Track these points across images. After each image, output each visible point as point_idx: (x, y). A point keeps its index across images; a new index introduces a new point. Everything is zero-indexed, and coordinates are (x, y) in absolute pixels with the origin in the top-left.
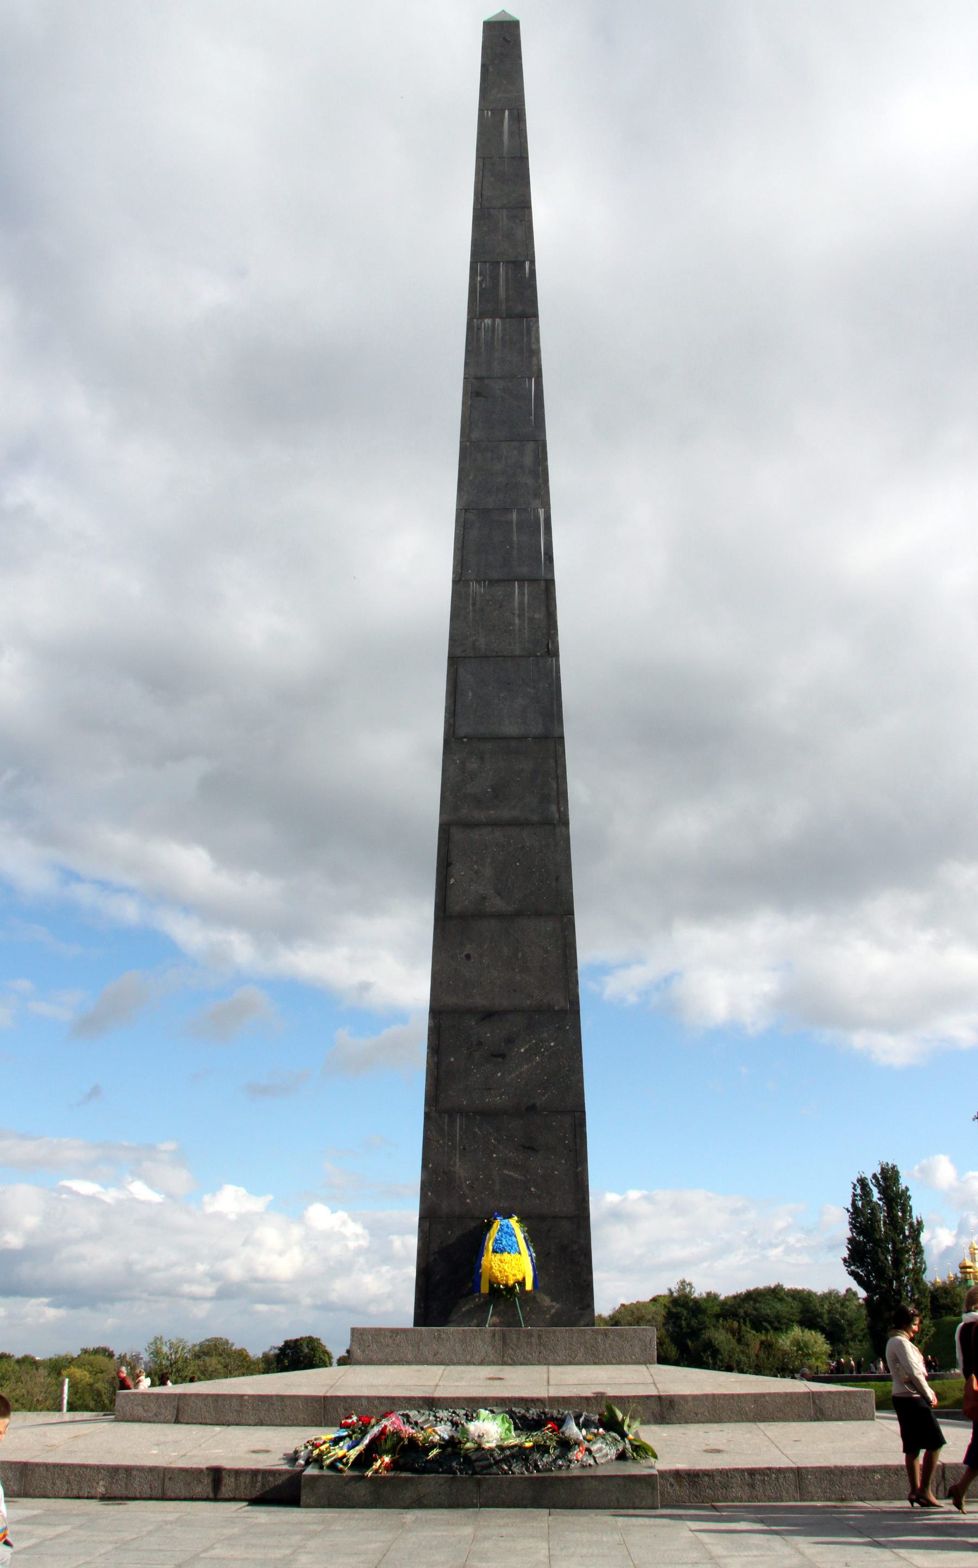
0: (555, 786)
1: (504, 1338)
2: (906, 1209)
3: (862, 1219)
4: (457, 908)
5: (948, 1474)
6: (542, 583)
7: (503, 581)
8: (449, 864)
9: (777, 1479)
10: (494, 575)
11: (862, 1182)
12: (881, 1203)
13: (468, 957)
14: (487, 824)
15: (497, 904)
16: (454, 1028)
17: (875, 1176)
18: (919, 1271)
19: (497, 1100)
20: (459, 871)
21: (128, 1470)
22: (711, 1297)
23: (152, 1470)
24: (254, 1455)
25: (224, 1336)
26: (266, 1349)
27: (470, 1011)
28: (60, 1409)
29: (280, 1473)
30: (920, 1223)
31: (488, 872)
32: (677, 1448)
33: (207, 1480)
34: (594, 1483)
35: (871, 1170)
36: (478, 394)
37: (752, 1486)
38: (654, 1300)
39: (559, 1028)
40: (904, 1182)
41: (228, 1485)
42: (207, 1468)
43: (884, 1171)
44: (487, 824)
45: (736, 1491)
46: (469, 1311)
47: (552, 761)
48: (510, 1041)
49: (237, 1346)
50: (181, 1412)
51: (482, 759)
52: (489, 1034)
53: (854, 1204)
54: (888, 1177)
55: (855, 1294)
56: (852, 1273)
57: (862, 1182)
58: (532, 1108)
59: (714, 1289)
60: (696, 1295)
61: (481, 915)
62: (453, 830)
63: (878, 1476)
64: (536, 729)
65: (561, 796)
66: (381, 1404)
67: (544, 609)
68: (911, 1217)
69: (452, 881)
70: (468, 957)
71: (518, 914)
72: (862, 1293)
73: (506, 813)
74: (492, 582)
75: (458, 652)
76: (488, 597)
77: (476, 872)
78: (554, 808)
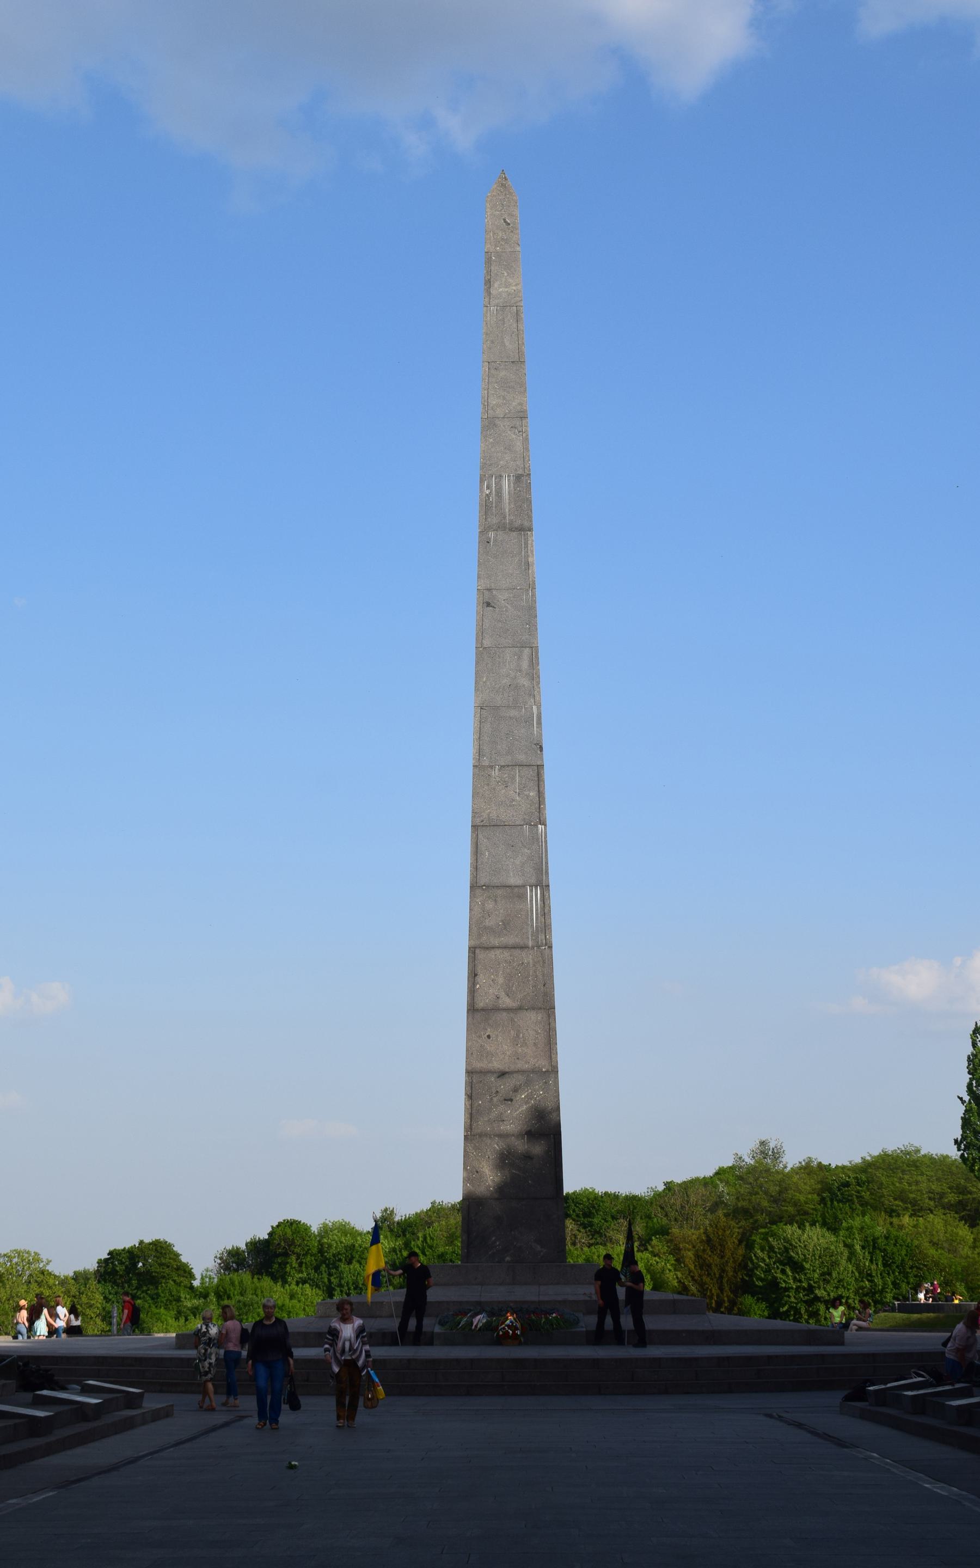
13: (489, 1037)
15: (506, 1002)
31: (501, 980)
36: (488, 605)
48: (516, 1090)
51: (496, 901)
52: (504, 1086)
61: (496, 1009)
62: (477, 951)
70: (489, 1037)
71: (520, 1008)
73: (511, 940)
75: (478, 821)
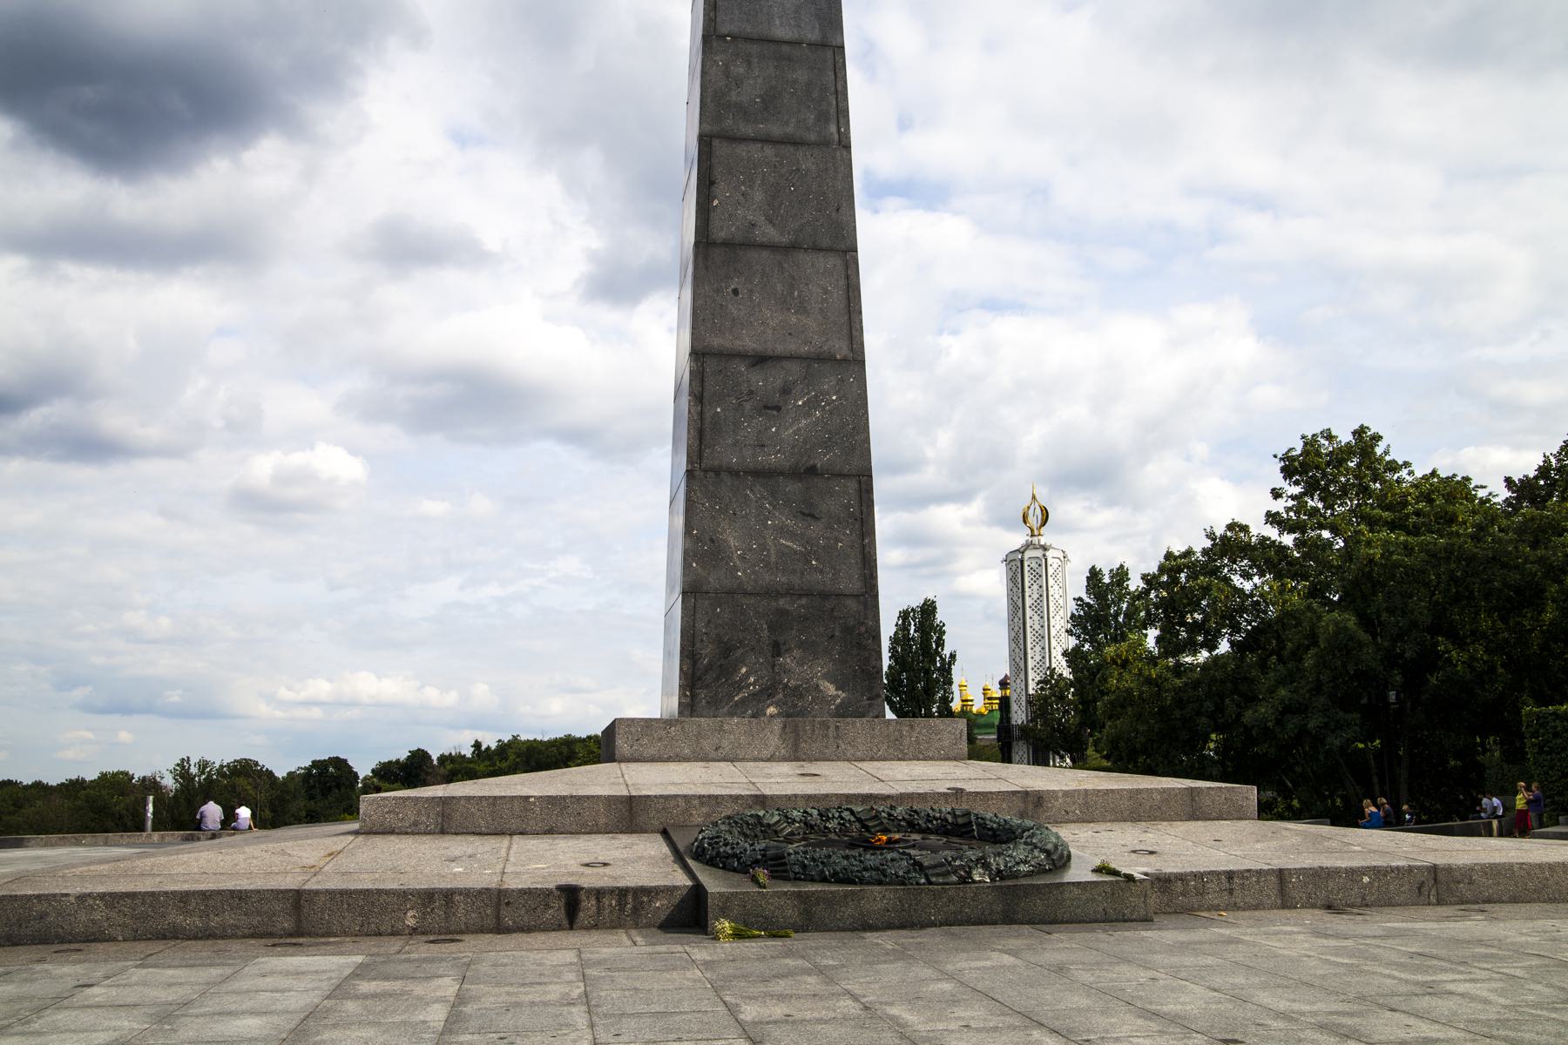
1: (796, 731)
4: (722, 234)
5: (1441, 877)
8: (712, 183)
9: (1258, 882)
13: (735, 292)
16: (713, 374)
19: (773, 459)
20: (723, 191)
21: (448, 895)
23: (484, 892)
24: (588, 870)
27: (741, 355)
28: (140, 827)
29: (670, 890)
31: (758, 196)
32: (1091, 848)
33: (558, 905)
34: (1076, 891)
35: (916, 602)
37: (1231, 892)
39: (842, 380)
40: (940, 617)
41: (588, 905)
42: (559, 888)
44: (755, 140)
45: (1212, 898)
46: (743, 701)
47: (831, 74)
48: (786, 391)
50: (447, 821)
51: (749, 63)
52: (761, 381)
54: (928, 609)
58: (812, 471)
62: (716, 143)
63: (1366, 879)
64: (813, 35)
65: (842, 114)
66: (702, 804)
69: (716, 202)
70: (735, 292)
71: (793, 247)
73: (776, 130)
78: (833, 128)
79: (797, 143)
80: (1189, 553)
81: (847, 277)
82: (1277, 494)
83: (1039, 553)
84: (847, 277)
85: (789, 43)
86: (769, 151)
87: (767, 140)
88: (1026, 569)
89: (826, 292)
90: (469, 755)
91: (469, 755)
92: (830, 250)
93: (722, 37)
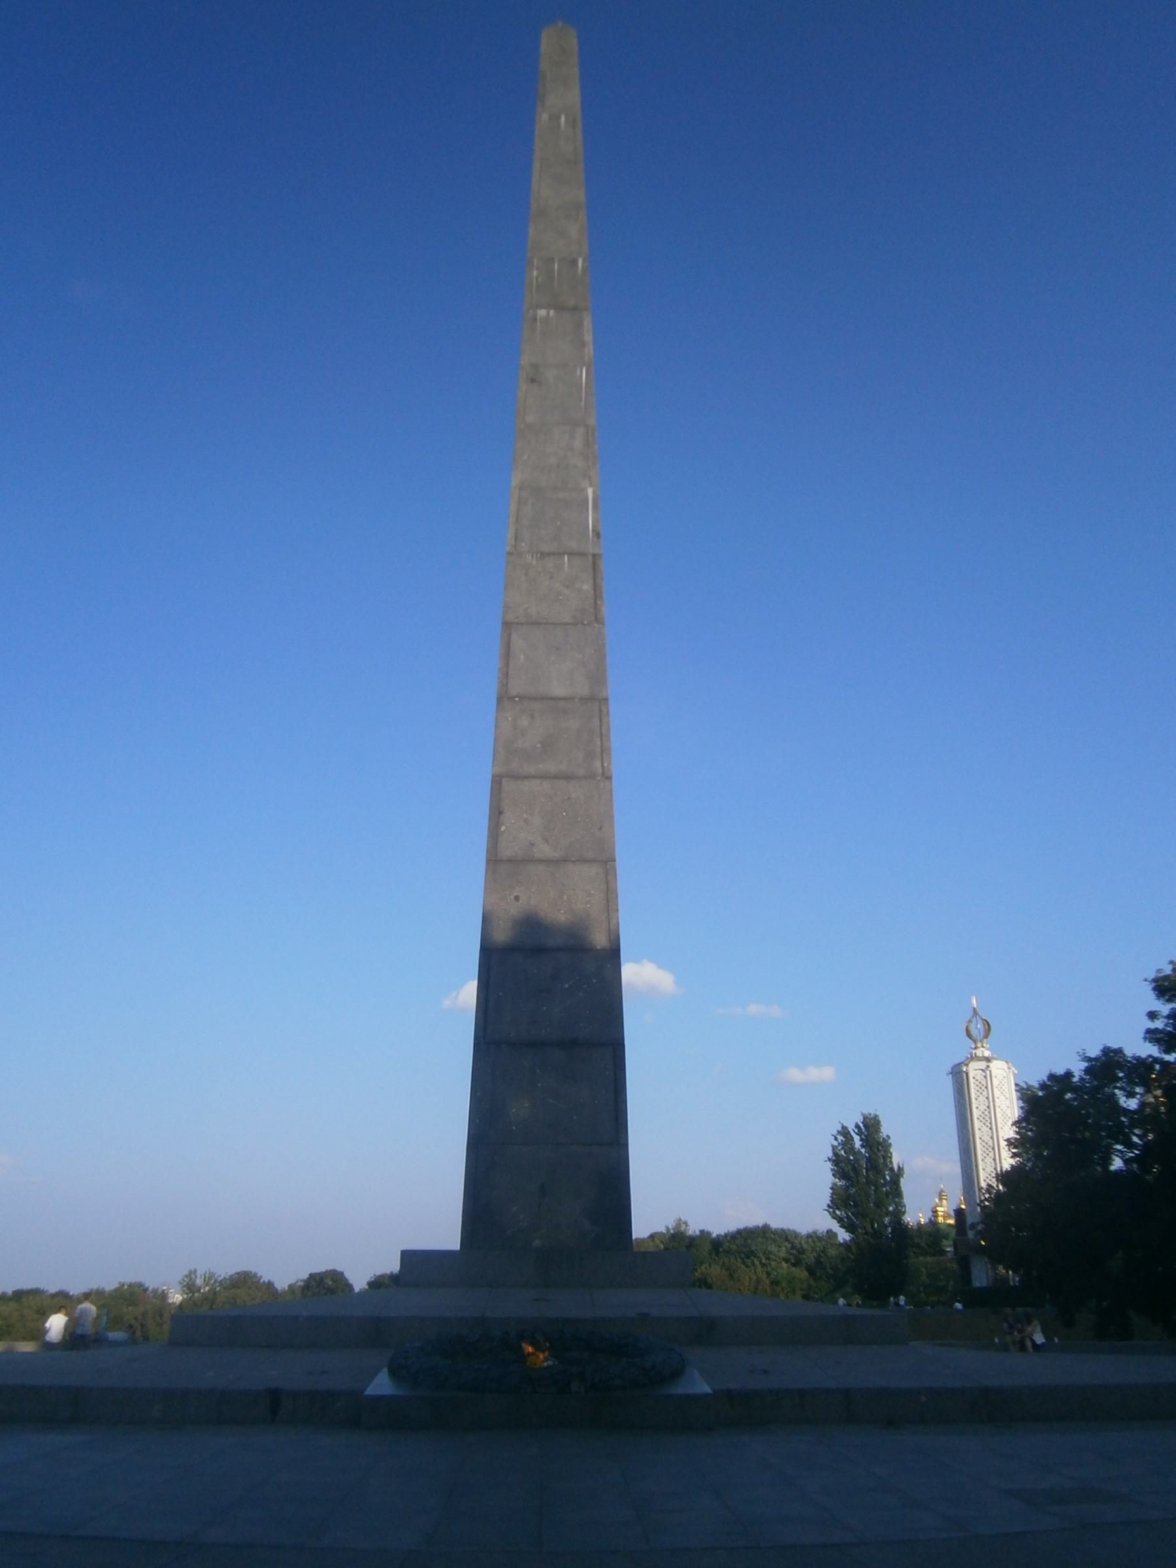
0: (599, 743)
2: (887, 1156)
3: (843, 1164)
6: (590, 558)
7: (554, 554)
8: (500, 813)
10: (546, 548)
11: (844, 1132)
12: (863, 1150)
14: (527, 777)
15: (545, 850)
17: (857, 1126)
18: (899, 1213)
22: (704, 1234)
25: (253, 1270)
26: (292, 1281)
30: (900, 1169)
35: (852, 1120)
38: (652, 1236)
40: (885, 1130)
43: (865, 1118)
44: (534, 777)
49: (265, 1279)
51: (532, 717)
53: (835, 1154)
54: (870, 1127)
55: (835, 1235)
56: (834, 1216)
57: (844, 1132)
59: (707, 1227)
60: (690, 1232)
62: (504, 781)
64: (583, 690)
67: (591, 581)
68: (891, 1162)
69: (503, 828)
71: (564, 860)
72: (843, 1235)
73: (551, 767)
74: (544, 555)
76: (540, 569)
77: (525, 821)
78: (598, 764)
79: (568, 777)
80: (1069, 1074)
81: (607, 882)
82: (1152, 1015)
83: (983, 1065)
84: (607, 882)
85: (565, 699)
86: (546, 785)
87: (544, 777)
88: (971, 1080)
89: (589, 895)
90: (357, 1290)
91: (357, 1290)
92: (593, 861)
93: (511, 698)
